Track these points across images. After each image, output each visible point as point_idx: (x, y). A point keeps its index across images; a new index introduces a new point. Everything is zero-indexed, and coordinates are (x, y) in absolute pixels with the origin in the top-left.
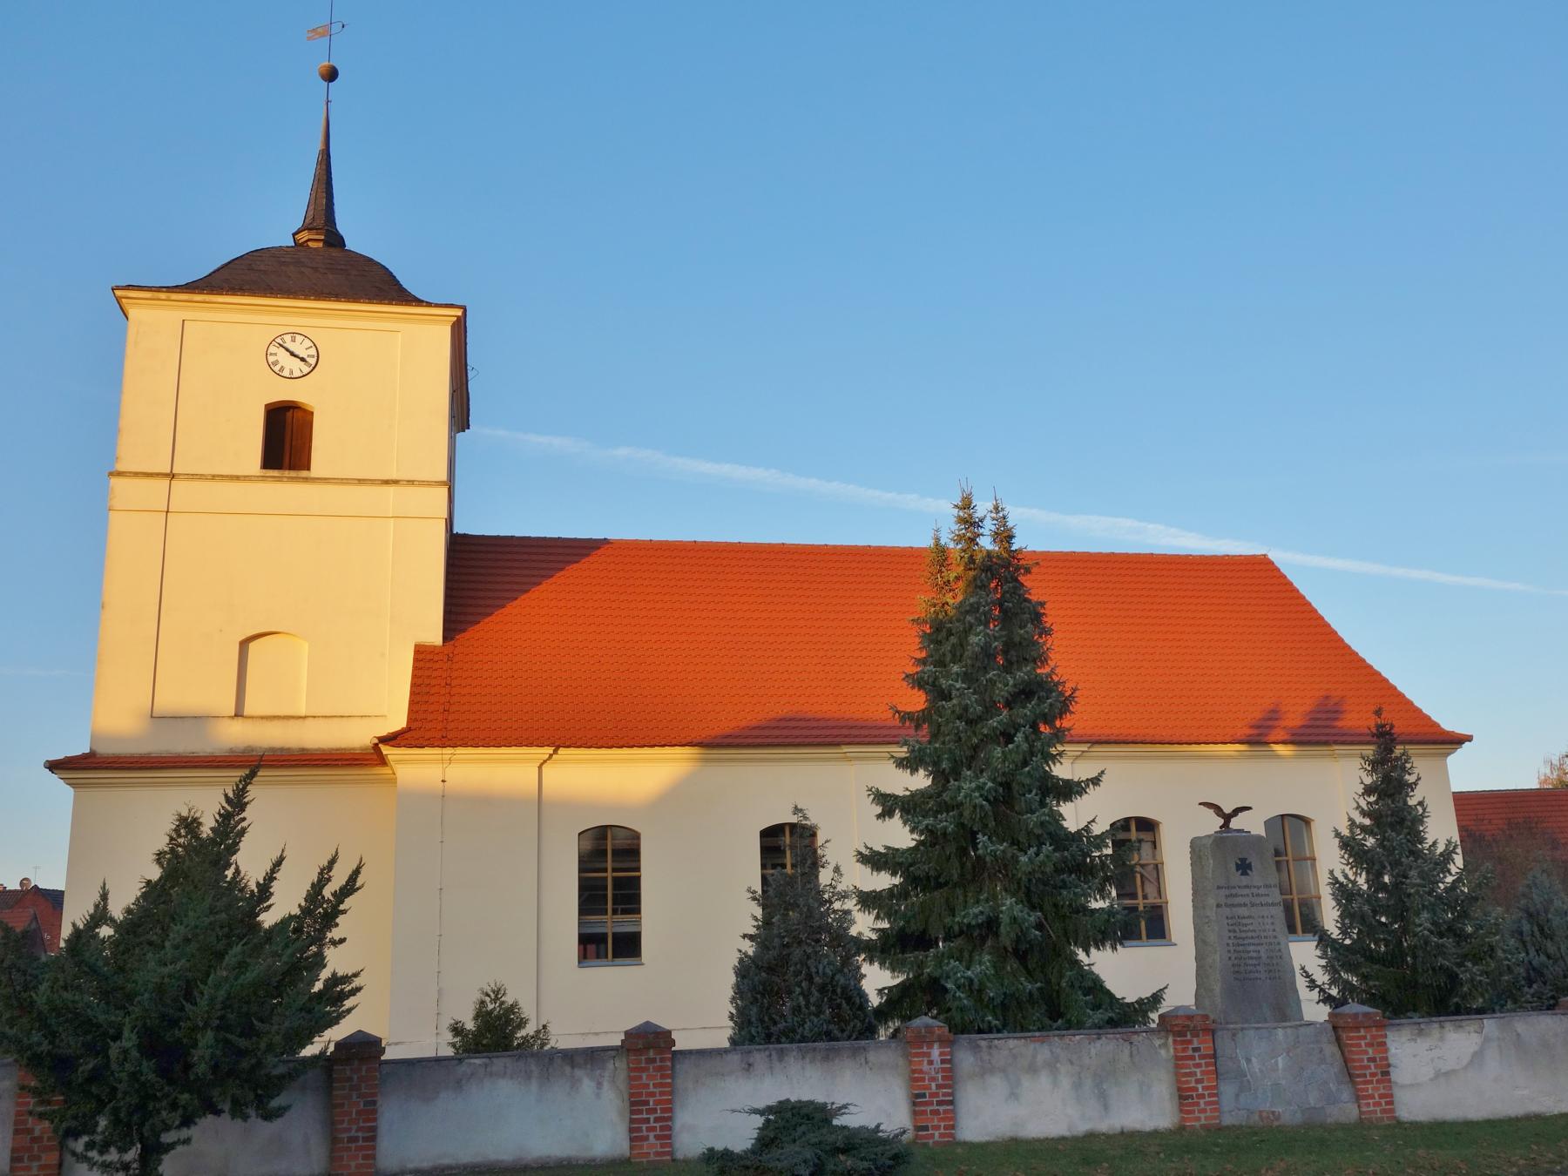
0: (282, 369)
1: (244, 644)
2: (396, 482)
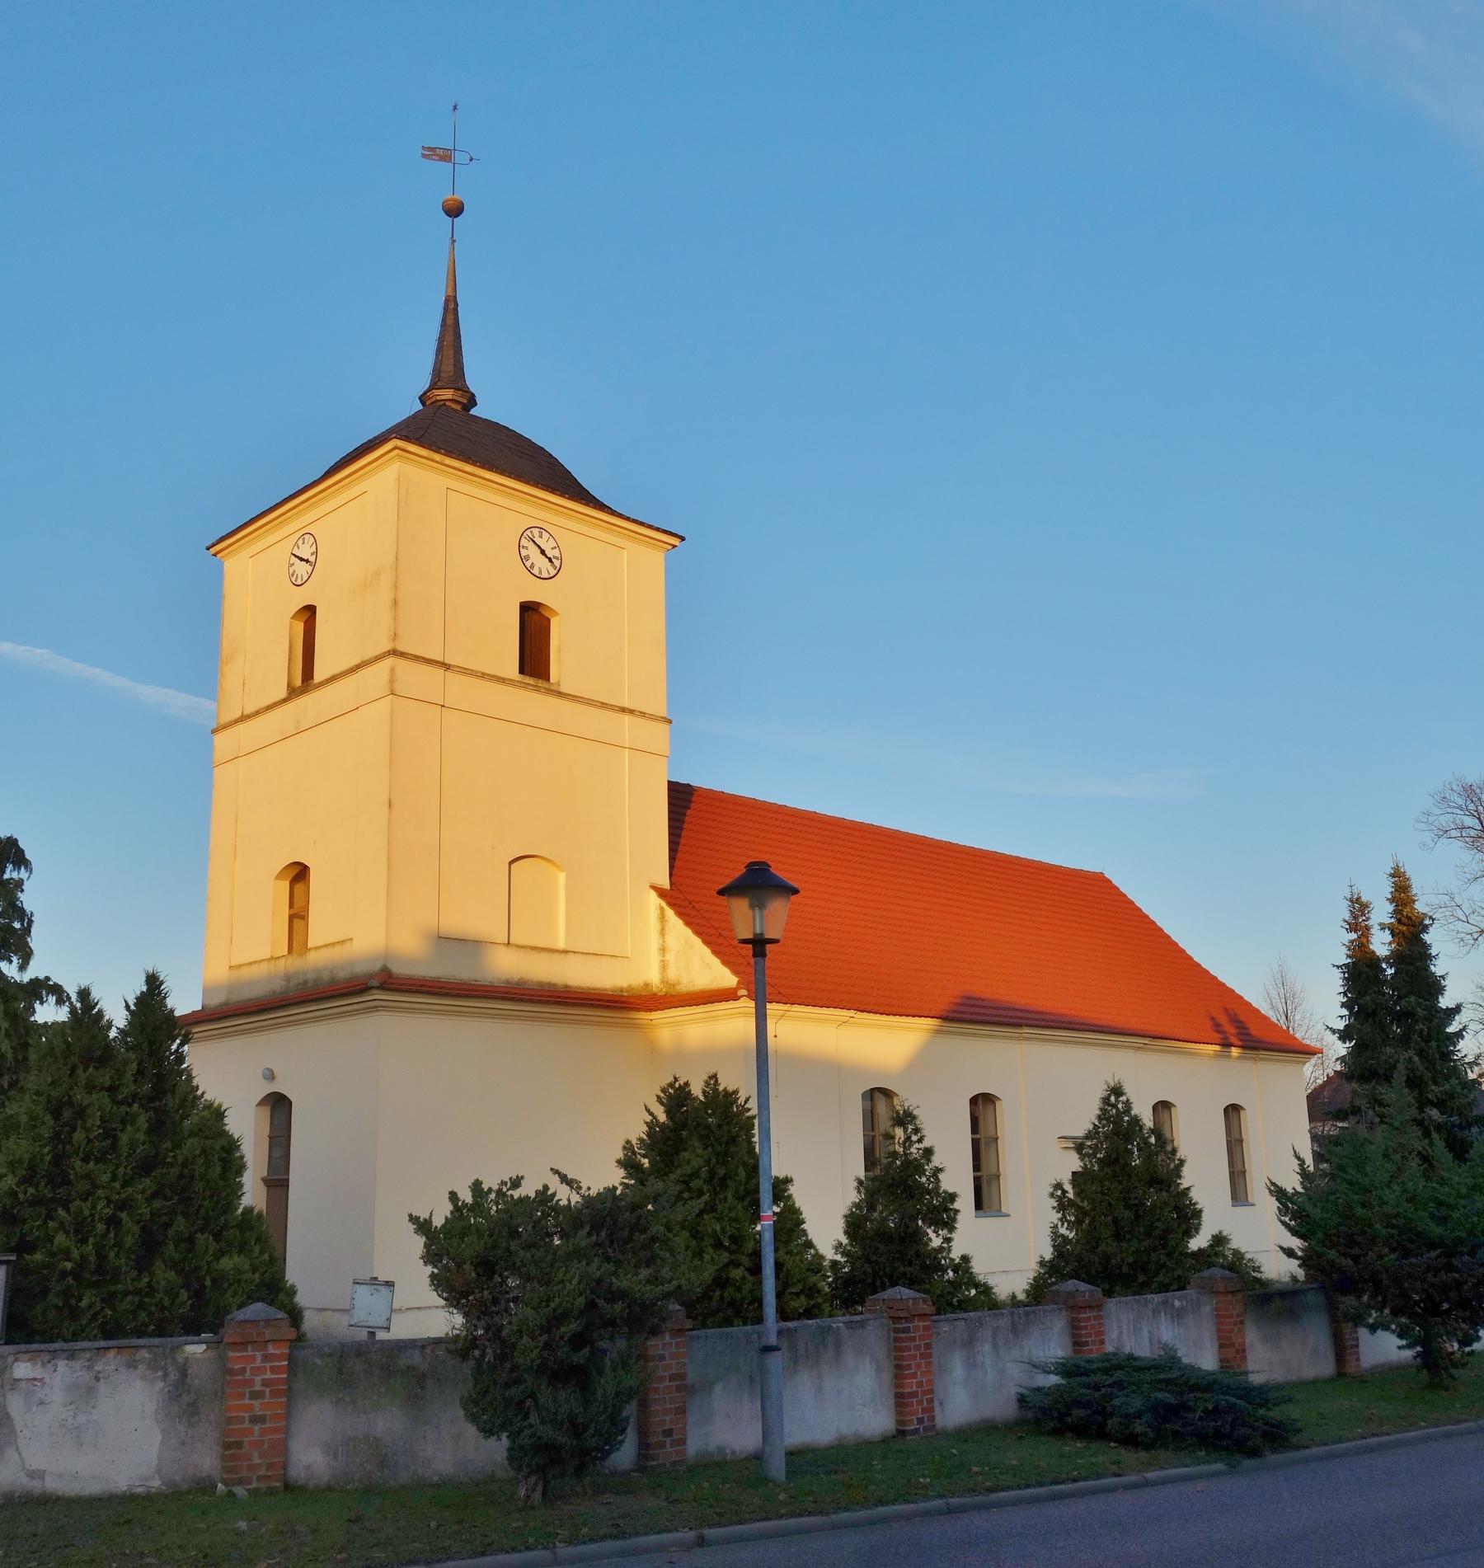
0: (532, 565)
1: (511, 863)
2: (631, 711)
